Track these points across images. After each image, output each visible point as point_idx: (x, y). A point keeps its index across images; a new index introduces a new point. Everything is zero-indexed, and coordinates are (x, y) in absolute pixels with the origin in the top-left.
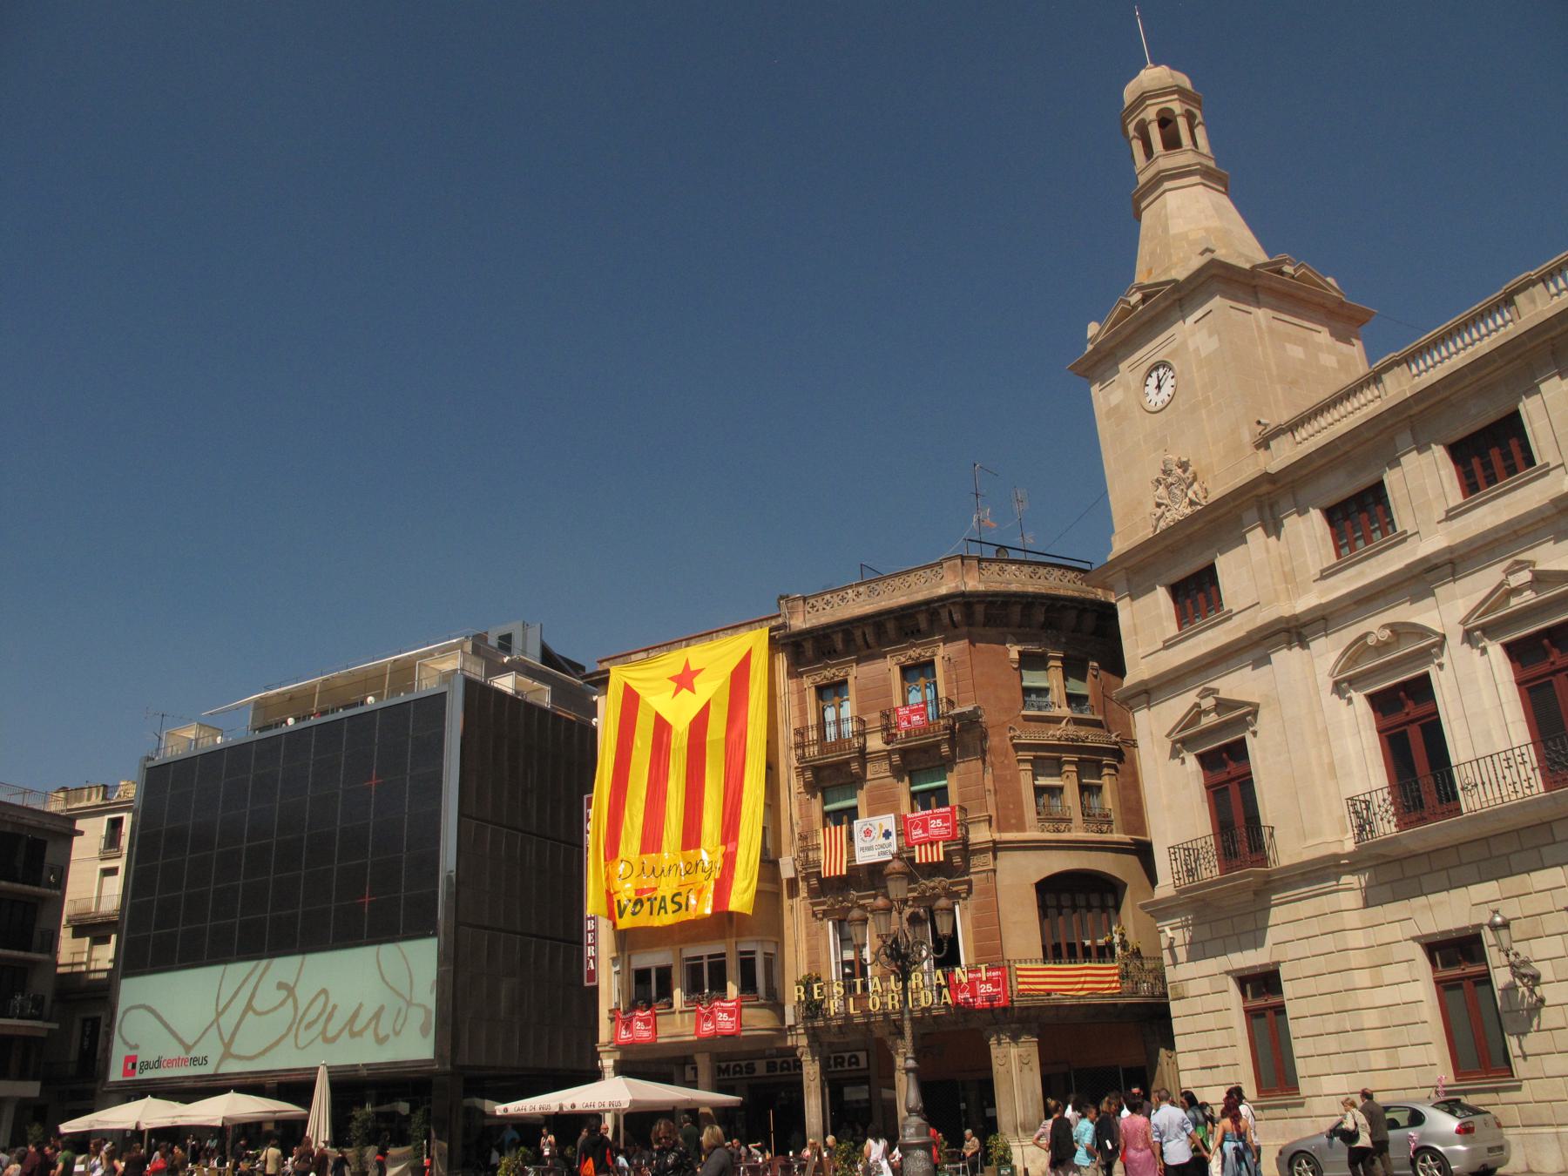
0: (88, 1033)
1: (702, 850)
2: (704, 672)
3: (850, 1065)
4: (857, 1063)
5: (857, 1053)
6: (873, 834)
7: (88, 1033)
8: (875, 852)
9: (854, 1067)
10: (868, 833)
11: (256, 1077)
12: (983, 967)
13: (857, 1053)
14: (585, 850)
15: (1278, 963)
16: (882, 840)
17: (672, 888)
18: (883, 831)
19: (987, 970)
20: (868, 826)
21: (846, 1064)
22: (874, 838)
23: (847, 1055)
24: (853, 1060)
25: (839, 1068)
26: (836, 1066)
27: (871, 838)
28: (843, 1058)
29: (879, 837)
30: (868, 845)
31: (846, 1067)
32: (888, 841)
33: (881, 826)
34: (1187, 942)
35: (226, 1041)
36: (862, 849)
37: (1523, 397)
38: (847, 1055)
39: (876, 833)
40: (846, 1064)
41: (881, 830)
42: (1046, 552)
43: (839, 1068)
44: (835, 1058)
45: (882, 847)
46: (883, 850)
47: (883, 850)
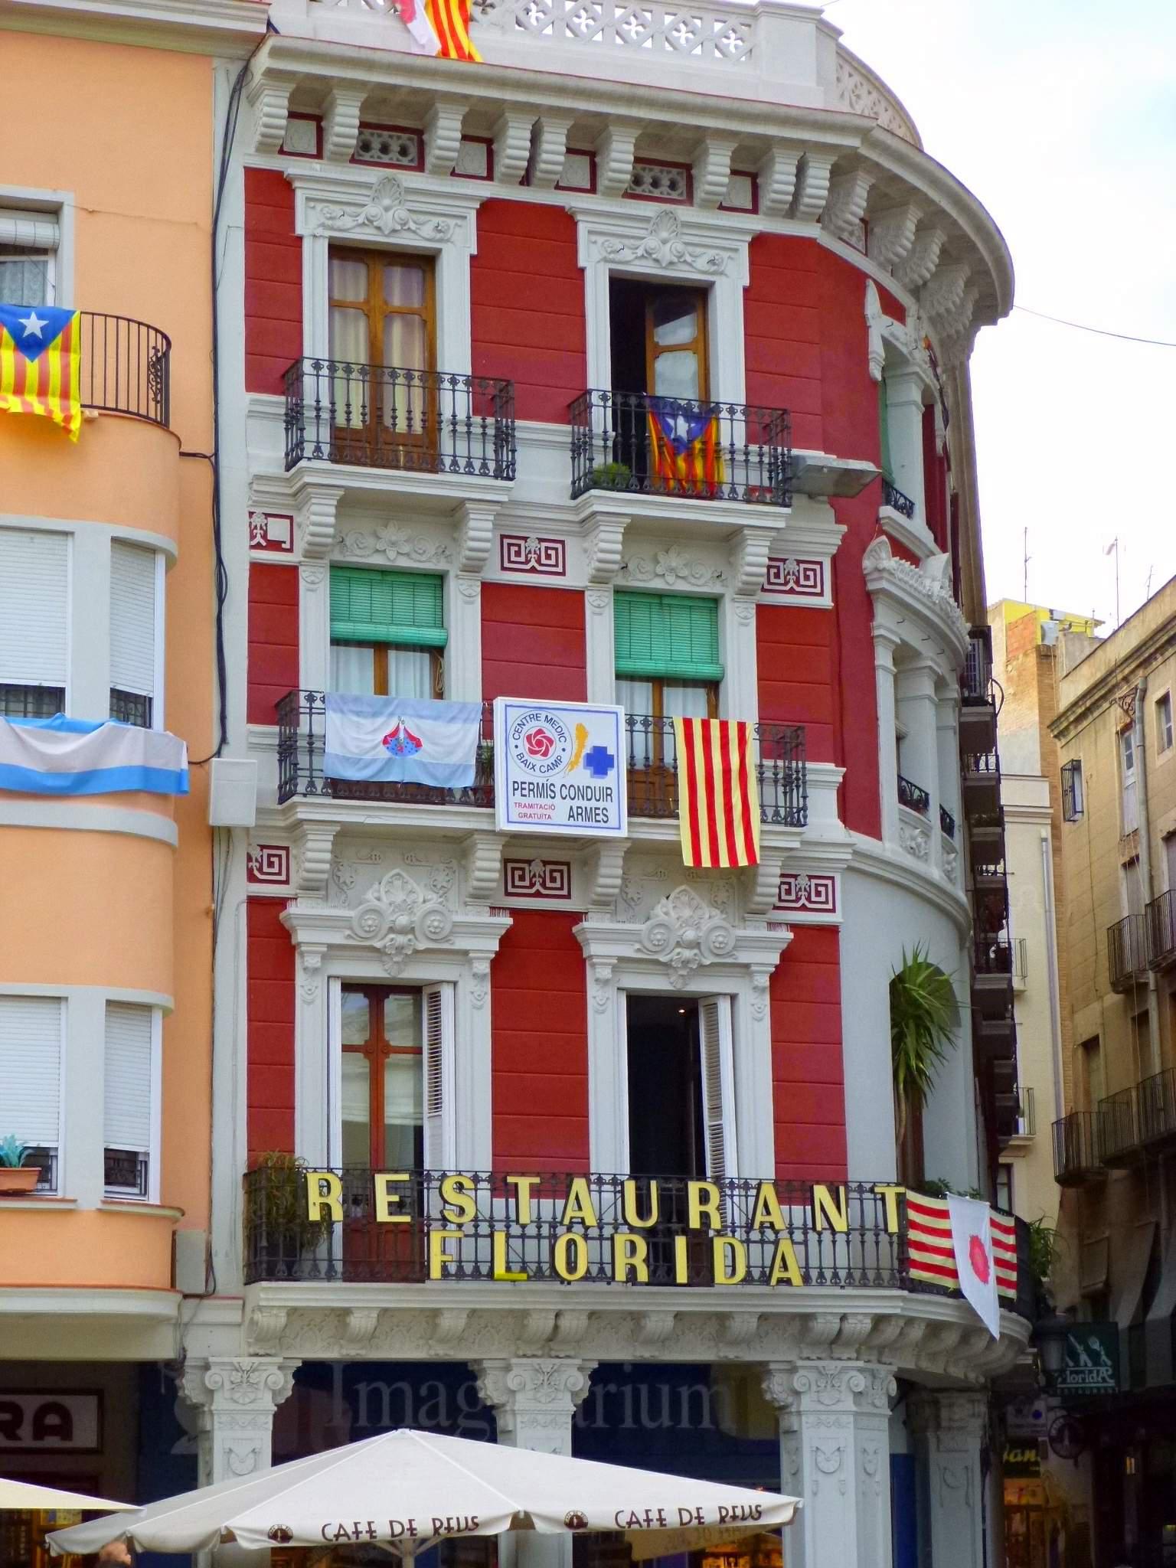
2: (406, 35)
4: (65, 1430)
5: (66, 1401)
6: (555, 751)
8: (560, 810)
9: (52, 1442)
10: (539, 744)
12: (524, 1184)
13: (66, 1401)
16: (583, 776)
17: (663, 906)
18: (587, 750)
19: (536, 1192)
20: (542, 724)
21: (26, 1431)
22: (558, 762)
23: (30, 1404)
24: (52, 1420)
27: (550, 760)
28: (17, 1411)
29: (572, 765)
30: (538, 778)
32: (599, 782)
33: (582, 732)
36: (518, 786)
37: (26, 334)
38: (30, 1404)
39: (568, 749)
40: (26, 1431)
41: (582, 746)
42: (209, 229)
45: (581, 792)
46: (584, 804)
47: (584, 804)
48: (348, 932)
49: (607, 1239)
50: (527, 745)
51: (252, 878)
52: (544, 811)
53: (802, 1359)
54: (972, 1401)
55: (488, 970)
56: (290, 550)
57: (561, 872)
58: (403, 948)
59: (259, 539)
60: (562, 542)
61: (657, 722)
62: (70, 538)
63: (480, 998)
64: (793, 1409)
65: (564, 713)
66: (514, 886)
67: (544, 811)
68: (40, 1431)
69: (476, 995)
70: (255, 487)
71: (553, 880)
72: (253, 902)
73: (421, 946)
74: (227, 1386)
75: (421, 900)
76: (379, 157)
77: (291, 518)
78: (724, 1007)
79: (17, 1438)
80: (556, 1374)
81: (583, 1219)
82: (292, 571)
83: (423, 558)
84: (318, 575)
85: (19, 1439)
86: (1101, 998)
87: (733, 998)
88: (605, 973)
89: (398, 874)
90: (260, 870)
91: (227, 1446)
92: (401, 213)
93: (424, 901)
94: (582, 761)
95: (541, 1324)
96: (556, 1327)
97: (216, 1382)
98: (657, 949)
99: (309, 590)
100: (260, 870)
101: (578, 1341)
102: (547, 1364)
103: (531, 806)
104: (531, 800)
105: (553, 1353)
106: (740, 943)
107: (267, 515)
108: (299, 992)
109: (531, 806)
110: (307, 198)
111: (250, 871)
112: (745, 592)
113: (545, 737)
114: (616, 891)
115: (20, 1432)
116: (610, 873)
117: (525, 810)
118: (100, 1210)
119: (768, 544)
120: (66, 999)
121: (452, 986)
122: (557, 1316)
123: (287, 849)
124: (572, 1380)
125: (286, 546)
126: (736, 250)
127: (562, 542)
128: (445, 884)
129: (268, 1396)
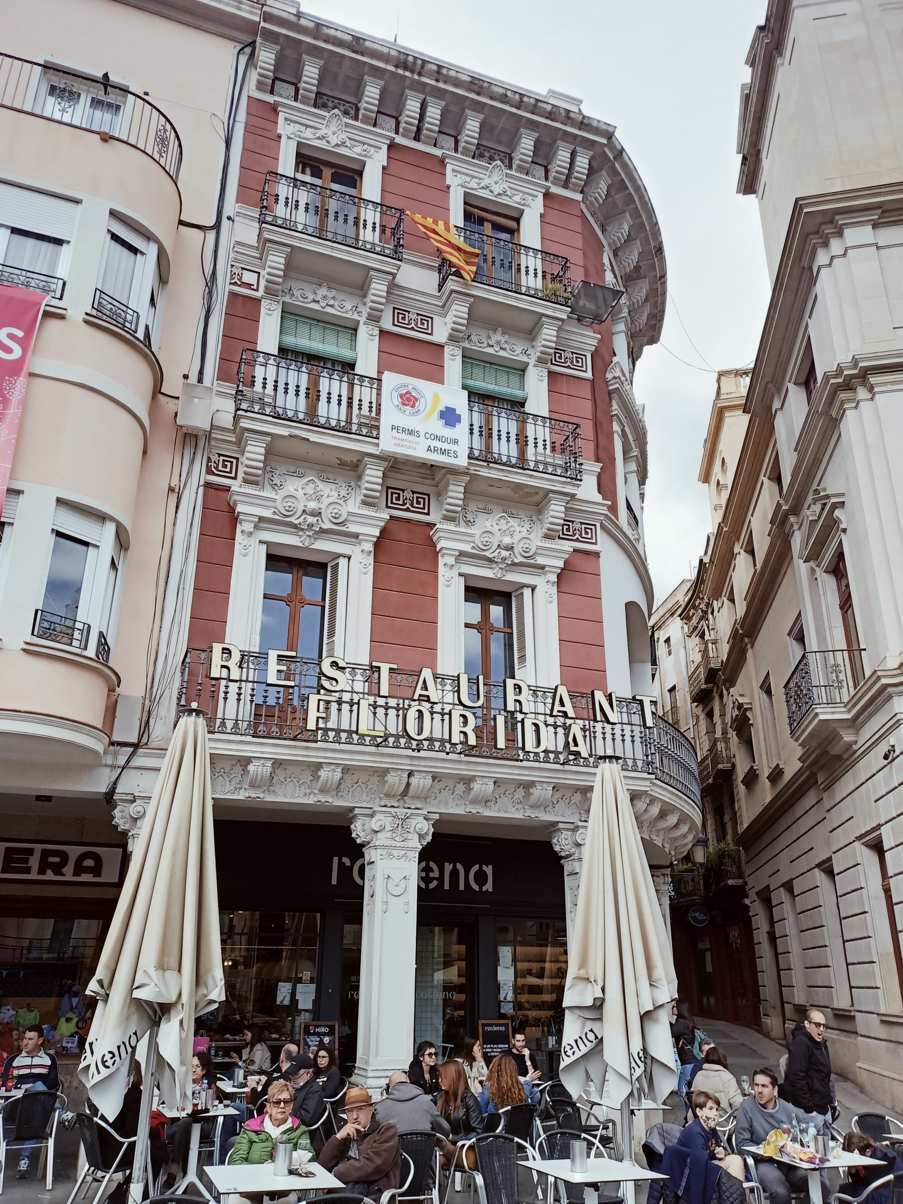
0: (277, 1036)
1: (267, 1119)
3: (77, 872)
4: (97, 871)
7: (277, 1036)
8: (424, 443)
9: (86, 878)
11: (846, 768)
14: (643, 190)
15: (573, 1161)
16: (438, 427)
23: (74, 852)
24: (89, 863)
25: (50, 876)
26: (41, 871)
28: (64, 856)
31: (68, 874)
32: (449, 432)
33: (436, 398)
34: (22, 380)
35: (132, 749)
38: (74, 852)
40: (69, 870)
43: (50, 876)
44: (45, 854)
48: (274, 510)
49: (447, 714)
51: (209, 471)
52: (412, 445)
53: (581, 821)
54: (664, 875)
55: (372, 549)
56: (257, 290)
57: (424, 499)
58: (313, 526)
59: (236, 280)
60: (432, 318)
61: (487, 433)
62: (80, 205)
64: (576, 856)
65: (425, 388)
66: (392, 503)
67: (412, 445)
68: (79, 869)
69: (363, 564)
70: (235, 249)
71: (418, 503)
72: (208, 485)
73: (325, 527)
75: (326, 495)
76: (329, 100)
77: (259, 273)
78: (527, 592)
79: (62, 874)
80: (408, 820)
81: (428, 697)
82: (258, 301)
83: (343, 310)
84: (274, 306)
87: (533, 588)
88: (451, 560)
89: (313, 480)
90: (217, 468)
92: (344, 136)
93: (328, 496)
94: (436, 414)
95: (395, 780)
96: (408, 785)
97: (138, 812)
98: (484, 548)
99: (267, 314)
100: (217, 468)
101: (425, 797)
102: (401, 812)
104: (404, 436)
105: (407, 806)
106: (539, 551)
107: (243, 269)
108: (237, 547)
109: (403, 440)
110: (285, 118)
112: (540, 361)
113: (414, 402)
114: (460, 509)
116: (456, 492)
117: (399, 442)
118: (24, 650)
119: (557, 329)
121: (346, 559)
122: (409, 775)
123: (237, 459)
124: (419, 826)
125: (255, 287)
126: (536, 196)
127: (432, 318)
128: (346, 495)
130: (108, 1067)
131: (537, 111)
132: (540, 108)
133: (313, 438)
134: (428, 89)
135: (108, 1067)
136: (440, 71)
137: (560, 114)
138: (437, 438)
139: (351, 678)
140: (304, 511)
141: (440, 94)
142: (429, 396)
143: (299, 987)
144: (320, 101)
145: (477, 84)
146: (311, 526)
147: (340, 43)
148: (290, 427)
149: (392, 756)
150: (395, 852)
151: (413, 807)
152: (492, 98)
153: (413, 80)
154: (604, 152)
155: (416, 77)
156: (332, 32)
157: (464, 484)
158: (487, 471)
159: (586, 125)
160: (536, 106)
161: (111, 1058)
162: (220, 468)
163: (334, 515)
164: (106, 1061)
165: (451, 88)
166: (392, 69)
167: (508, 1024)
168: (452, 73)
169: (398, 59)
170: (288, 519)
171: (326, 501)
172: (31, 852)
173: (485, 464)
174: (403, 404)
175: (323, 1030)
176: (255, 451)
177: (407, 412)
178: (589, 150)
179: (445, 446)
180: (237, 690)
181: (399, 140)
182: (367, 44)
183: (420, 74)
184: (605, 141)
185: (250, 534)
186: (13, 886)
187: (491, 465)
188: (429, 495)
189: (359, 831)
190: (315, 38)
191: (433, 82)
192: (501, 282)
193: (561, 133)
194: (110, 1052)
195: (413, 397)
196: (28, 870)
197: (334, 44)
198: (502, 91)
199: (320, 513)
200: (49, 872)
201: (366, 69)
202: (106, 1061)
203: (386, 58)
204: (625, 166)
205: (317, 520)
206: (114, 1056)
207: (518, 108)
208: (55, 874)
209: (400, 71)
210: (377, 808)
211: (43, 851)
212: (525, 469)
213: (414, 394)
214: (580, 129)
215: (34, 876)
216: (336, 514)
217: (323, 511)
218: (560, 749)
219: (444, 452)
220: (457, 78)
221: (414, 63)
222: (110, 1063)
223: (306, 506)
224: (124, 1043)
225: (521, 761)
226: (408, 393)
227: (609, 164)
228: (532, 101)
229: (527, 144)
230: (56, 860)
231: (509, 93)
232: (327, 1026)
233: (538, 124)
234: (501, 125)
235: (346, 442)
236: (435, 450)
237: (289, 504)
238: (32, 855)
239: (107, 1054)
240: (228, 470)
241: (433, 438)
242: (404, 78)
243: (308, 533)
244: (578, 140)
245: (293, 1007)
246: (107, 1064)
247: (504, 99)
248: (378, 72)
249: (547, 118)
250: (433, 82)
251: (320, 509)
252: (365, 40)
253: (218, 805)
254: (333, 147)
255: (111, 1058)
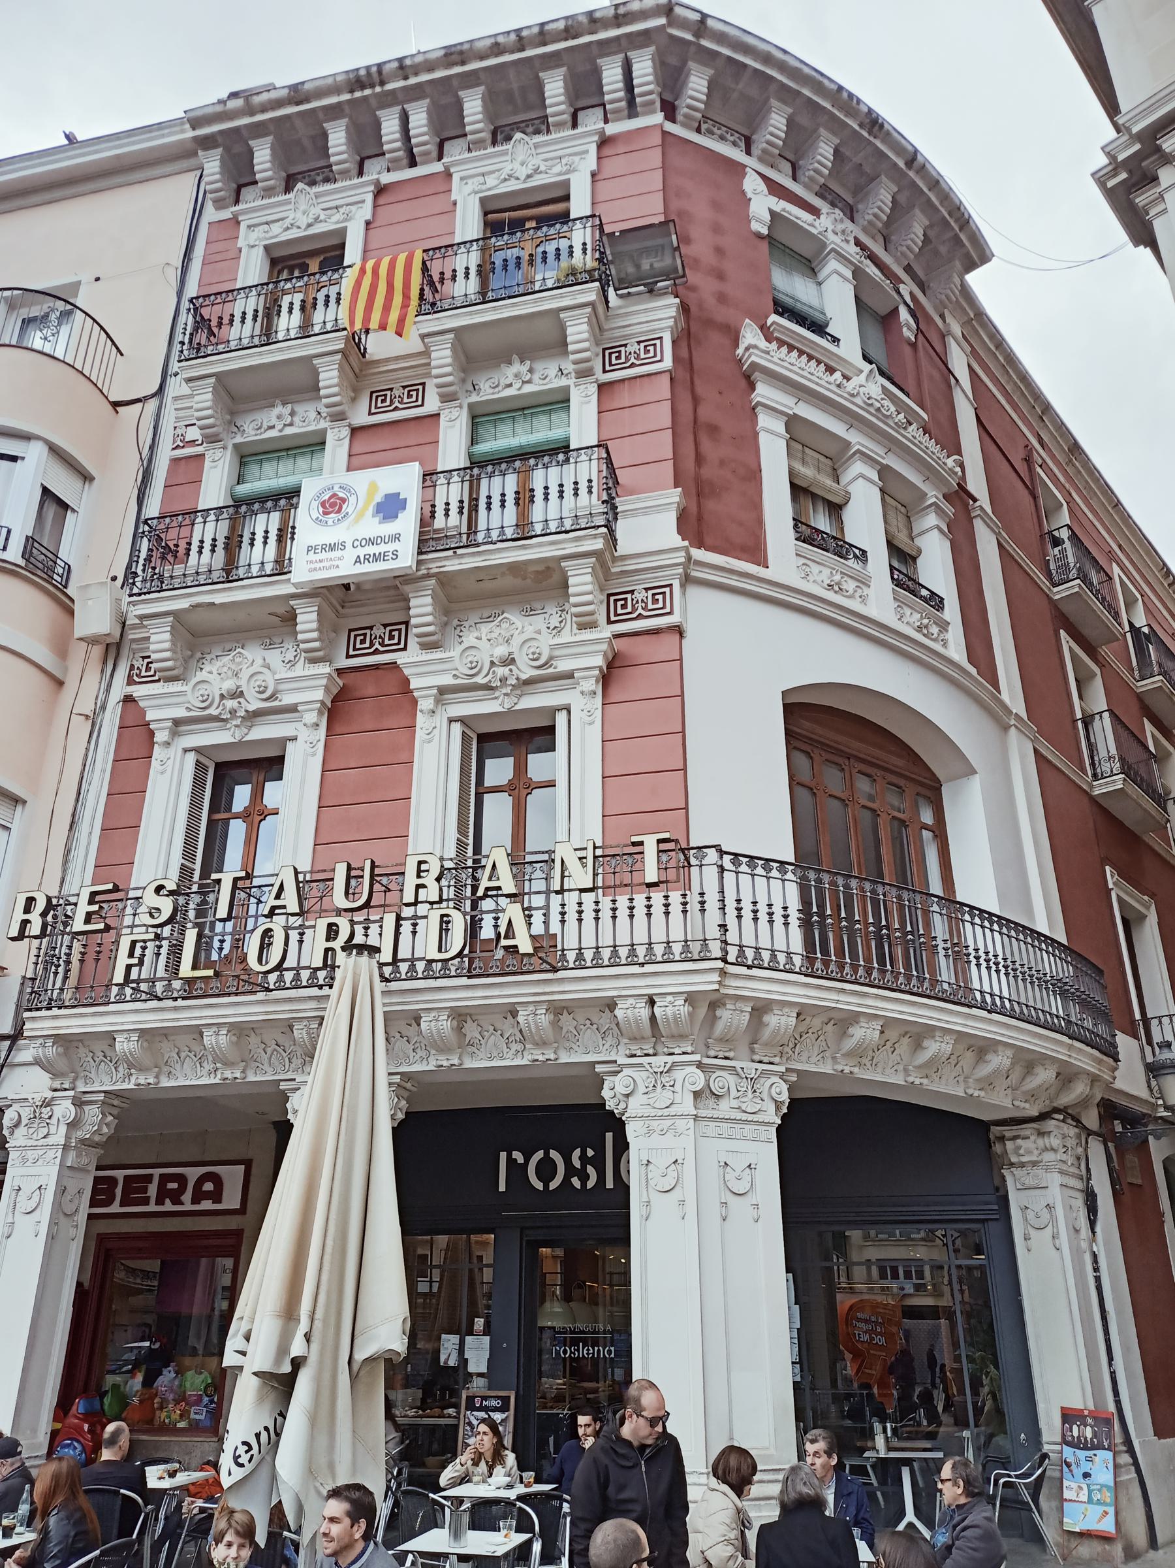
4: (217, 1196)
9: (207, 1205)
16: (374, 527)
18: (379, 498)
23: (193, 1174)
24: (208, 1186)
25: (168, 1206)
26: (159, 1202)
28: (182, 1180)
40: (187, 1197)
43: (168, 1206)
44: (164, 1179)
50: (332, 515)
63: (313, 745)
68: (197, 1198)
73: (251, 708)
74: (733, 1093)
85: (182, 1204)
86: (524, 579)
91: (723, 1160)
94: (371, 509)
95: (632, 1011)
103: (321, 561)
109: (321, 561)
111: (130, 676)
115: (183, 1198)
120: (24, 802)
129: (772, 1107)
130: (242, 1465)
131: (548, 37)
132: (549, 32)
133: (219, 599)
134: (400, 96)
135: (242, 1465)
136: (403, 68)
137: (580, 23)
138: (371, 542)
139: (698, 863)
140: (492, 663)
141: (415, 93)
142: (362, 490)
143: (469, 1339)
144: (499, 135)
145: (455, 55)
146: (504, 680)
147: (278, 104)
148: (190, 595)
149: (290, 1000)
150: (654, 1124)
151: (677, 1051)
152: (482, 58)
153: (375, 95)
154: (672, 37)
155: (378, 89)
156: (265, 97)
157: (430, 592)
158: (457, 561)
159: (624, 15)
160: (543, 35)
161: (247, 1452)
162: (650, 606)
163: (531, 656)
164: (239, 1456)
165: (424, 77)
166: (347, 97)
167: (509, 1397)
168: (419, 59)
169: (349, 81)
170: (206, 712)
171: (245, 675)
172: (149, 1179)
173: (450, 553)
174: (339, 511)
175: (493, 1403)
176: (160, 640)
177: (330, 522)
178: (647, 46)
179: (382, 548)
180: (628, 904)
181: (611, 129)
182: (307, 86)
183: (382, 83)
184: (662, 21)
185: (167, 744)
186: (133, 1221)
187: (459, 551)
188: (609, 596)
189: (611, 1095)
190: (252, 114)
191: (401, 84)
192: (502, 291)
193: (594, 48)
194: (244, 1443)
195: (330, 498)
196: (146, 1202)
197: (273, 109)
198: (489, 42)
199: (513, 660)
200: (168, 1201)
201: (321, 115)
202: (239, 1456)
203: (335, 89)
204: (721, 38)
205: (511, 670)
206: (250, 1448)
207: (522, 49)
208: (173, 1204)
209: (358, 94)
210: (622, 1060)
211: (126, 1177)
212: (531, 537)
213: (326, 497)
214: (619, 26)
215: (152, 1208)
216: (534, 653)
217: (244, 689)
218: (318, 963)
219: (376, 558)
220: (426, 61)
221: (369, 74)
222: (244, 1459)
223: (492, 656)
224: (266, 1429)
225: (642, 965)
226: (334, 495)
227: (693, 49)
228: (536, 30)
229: (555, 87)
230: (174, 1186)
231: (501, 39)
232: (498, 1397)
233: (556, 54)
234: (515, 86)
235: (263, 589)
236: (367, 558)
237: (470, 659)
238: (151, 1182)
239: (240, 1446)
240: (660, 605)
241: (363, 543)
242: (365, 98)
243: (504, 691)
244: (624, 42)
245: (461, 1373)
246: (240, 1460)
247: (497, 49)
248: (334, 112)
249: (566, 39)
250: (401, 84)
251: (238, 687)
252: (303, 83)
253: (405, 1085)
254: (525, 181)
255: (247, 1452)
